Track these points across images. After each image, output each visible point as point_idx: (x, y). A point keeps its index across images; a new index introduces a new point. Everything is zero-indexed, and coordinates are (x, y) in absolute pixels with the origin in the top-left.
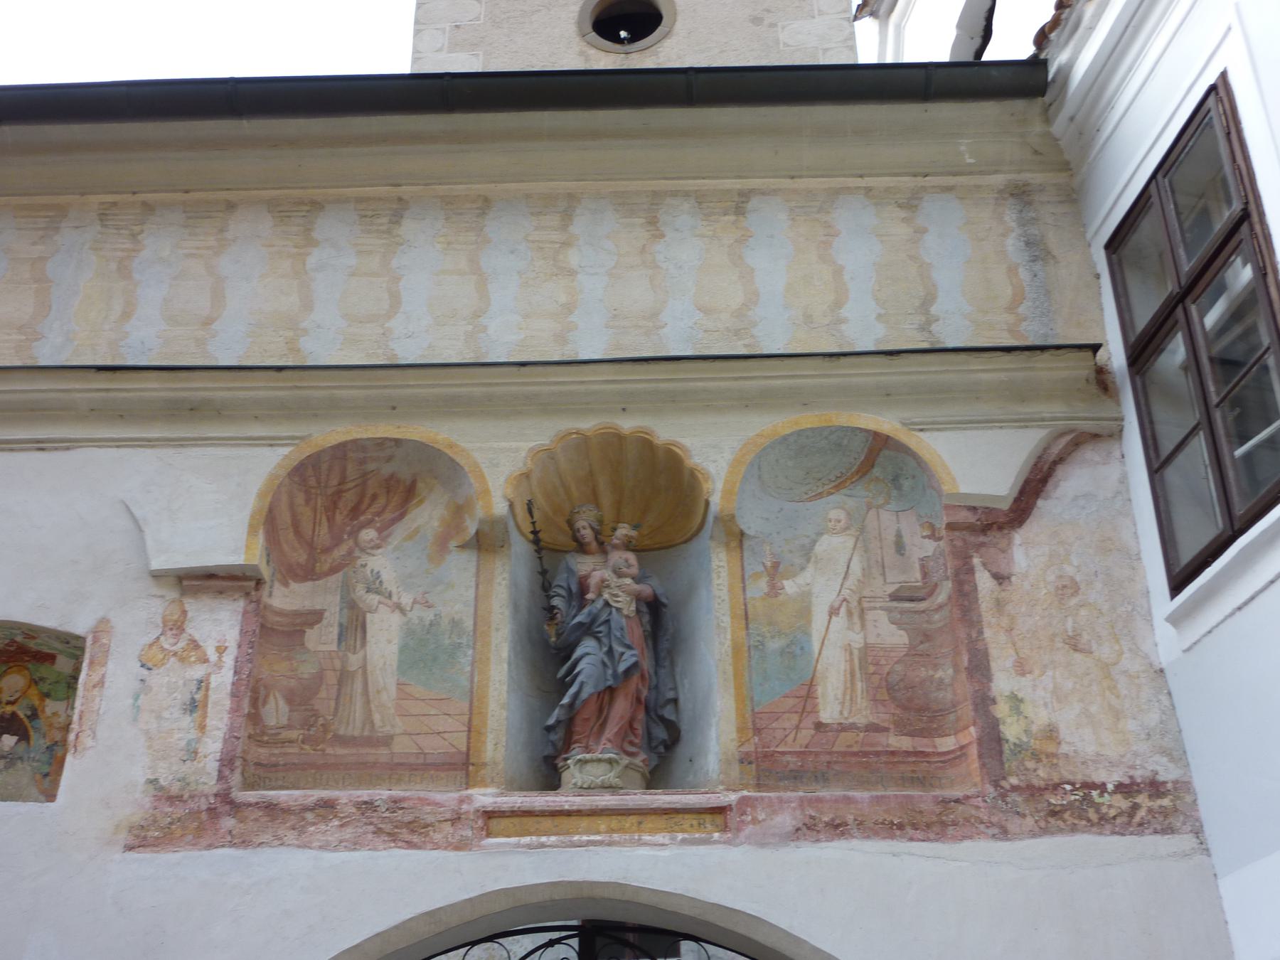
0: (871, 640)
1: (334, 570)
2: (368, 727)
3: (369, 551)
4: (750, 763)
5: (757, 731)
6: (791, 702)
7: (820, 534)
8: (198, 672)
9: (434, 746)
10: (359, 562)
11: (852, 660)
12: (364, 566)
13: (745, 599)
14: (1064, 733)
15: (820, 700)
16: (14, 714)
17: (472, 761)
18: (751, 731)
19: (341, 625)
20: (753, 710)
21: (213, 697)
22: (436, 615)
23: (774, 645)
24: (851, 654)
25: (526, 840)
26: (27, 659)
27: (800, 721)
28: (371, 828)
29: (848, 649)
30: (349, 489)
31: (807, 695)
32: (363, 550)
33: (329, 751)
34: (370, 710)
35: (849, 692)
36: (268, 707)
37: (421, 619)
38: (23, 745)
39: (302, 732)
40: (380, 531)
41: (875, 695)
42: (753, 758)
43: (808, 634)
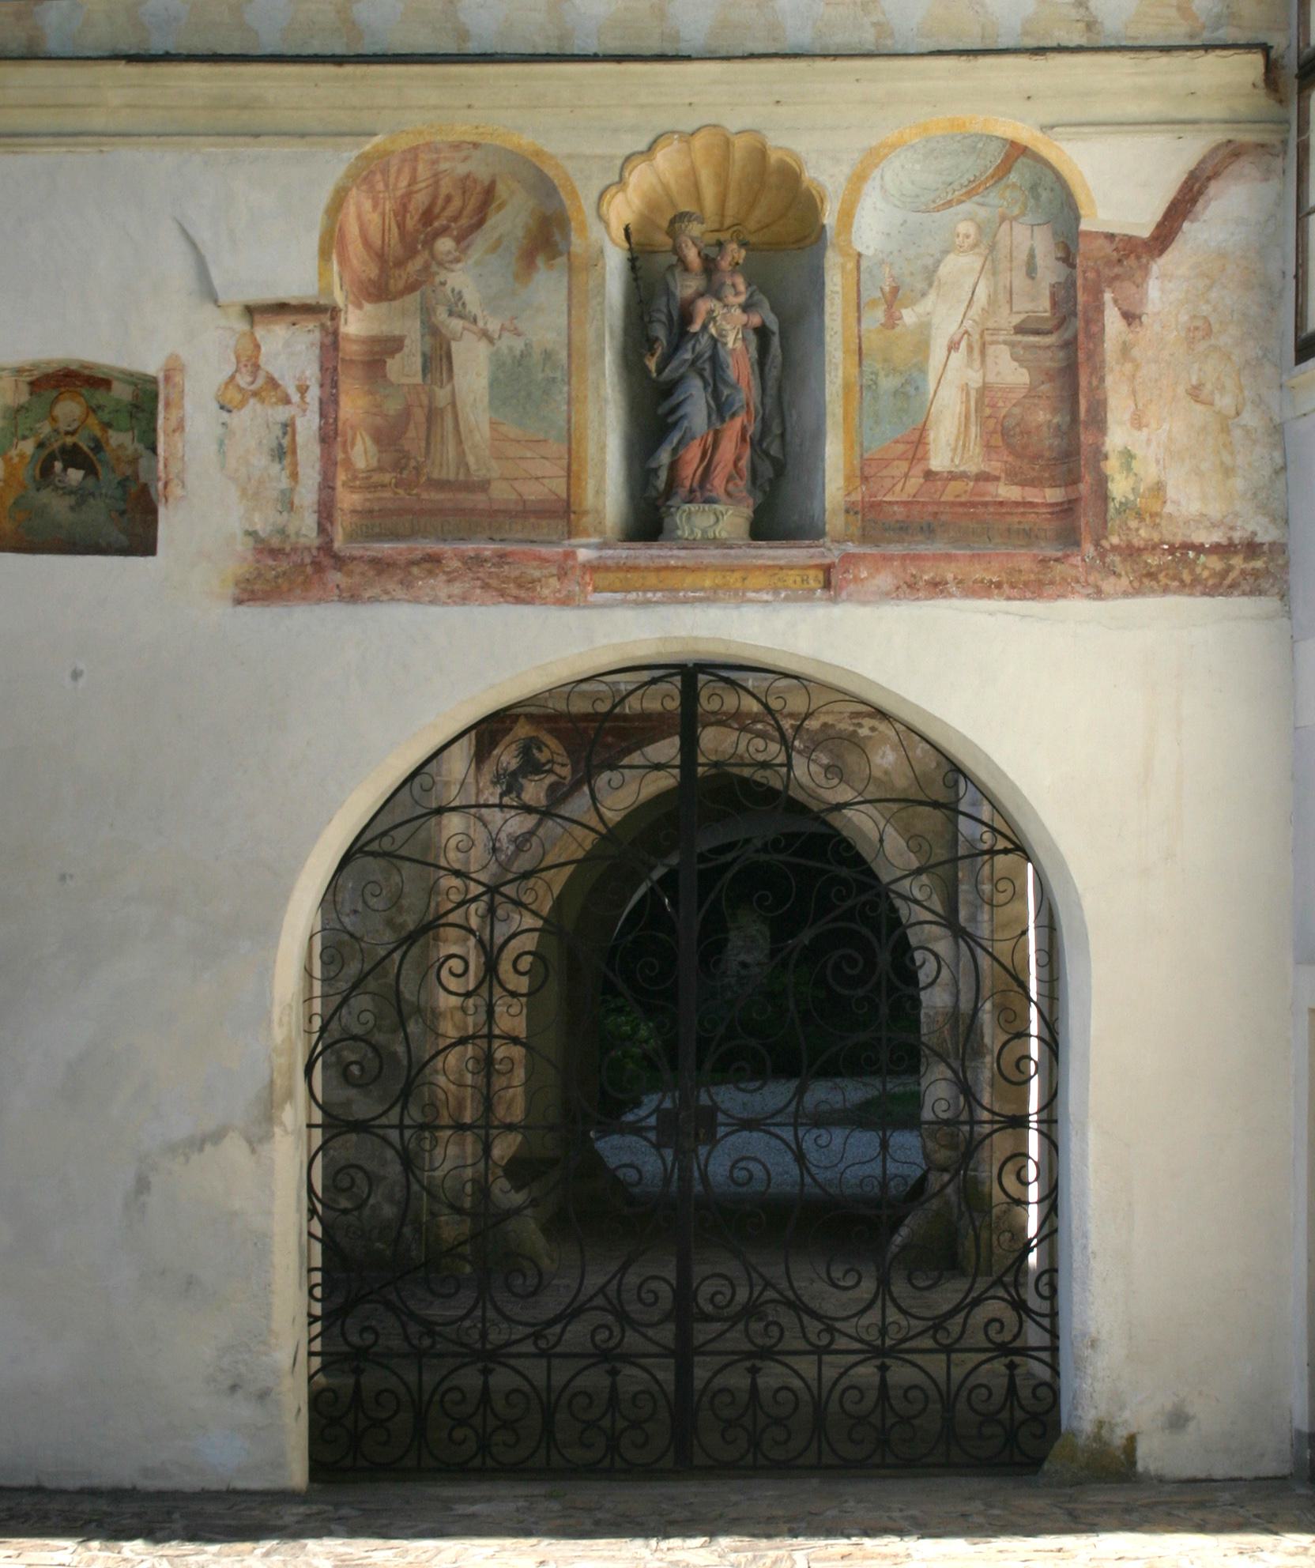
0: (991, 378)
1: (411, 288)
2: (462, 470)
3: (447, 265)
4: (856, 513)
5: (865, 479)
6: (901, 447)
7: (946, 252)
8: (282, 413)
9: (533, 492)
10: (438, 279)
11: (968, 400)
12: (443, 284)
13: (859, 331)
14: (1171, 493)
15: (932, 447)
16: (75, 445)
17: (573, 508)
18: (858, 479)
19: (424, 355)
20: (862, 456)
21: (299, 439)
22: (526, 345)
23: (887, 383)
24: (968, 394)
25: (633, 596)
26: (78, 383)
27: (910, 469)
28: (479, 583)
29: (965, 388)
30: (420, 190)
31: (917, 444)
32: (440, 264)
33: (425, 496)
34: (463, 452)
35: (962, 437)
36: (356, 448)
37: (511, 349)
38: (91, 482)
39: (393, 474)
40: (459, 240)
41: (988, 441)
42: (859, 508)
43: (923, 371)
